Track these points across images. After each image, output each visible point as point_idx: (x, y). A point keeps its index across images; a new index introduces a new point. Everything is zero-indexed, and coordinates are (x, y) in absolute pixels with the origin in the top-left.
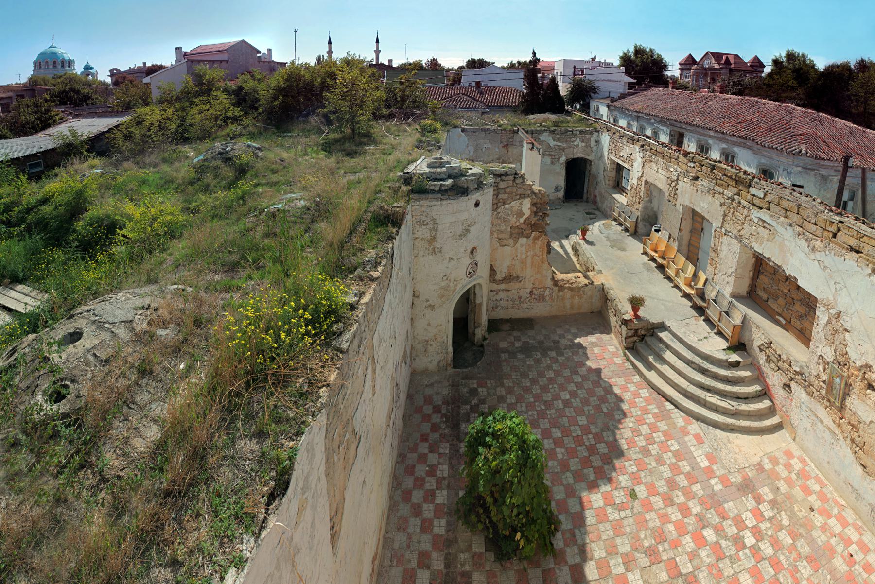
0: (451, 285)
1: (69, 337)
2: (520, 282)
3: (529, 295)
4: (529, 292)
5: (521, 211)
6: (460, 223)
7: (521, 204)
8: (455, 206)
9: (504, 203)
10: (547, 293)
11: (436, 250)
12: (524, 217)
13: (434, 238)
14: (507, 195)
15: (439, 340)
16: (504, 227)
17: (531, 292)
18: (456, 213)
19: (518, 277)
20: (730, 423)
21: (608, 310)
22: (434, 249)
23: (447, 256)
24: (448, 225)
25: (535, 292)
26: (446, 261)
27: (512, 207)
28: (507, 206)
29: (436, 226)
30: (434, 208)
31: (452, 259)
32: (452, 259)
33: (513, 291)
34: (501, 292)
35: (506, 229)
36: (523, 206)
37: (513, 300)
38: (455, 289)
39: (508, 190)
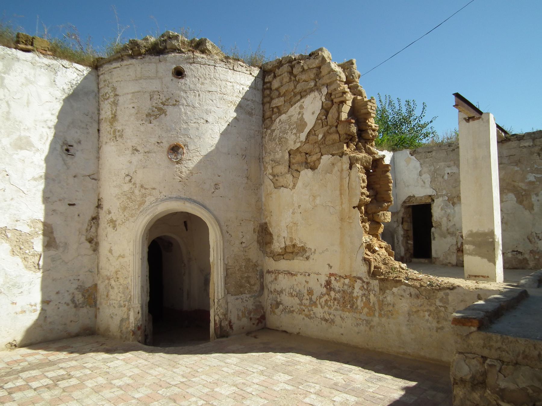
0: (137, 192)
1: (52, 252)
3: (324, 290)
4: (324, 283)
6: (147, 96)
8: (139, 69)
10: (357, 291)
12: (307, 130)
13: (115, 116)
14: (282, 99)
15: (121, 280)
17: (328, 283)
19: (303, 249)
21: (79, 84)
25: (335, 284)
27: (290, 117)
30: (115, 72)
31: (137, 151)
32: (137, 151)
35: (283, 157)
36: (304, 111)
37: (299, 295)
38: (143, 203)
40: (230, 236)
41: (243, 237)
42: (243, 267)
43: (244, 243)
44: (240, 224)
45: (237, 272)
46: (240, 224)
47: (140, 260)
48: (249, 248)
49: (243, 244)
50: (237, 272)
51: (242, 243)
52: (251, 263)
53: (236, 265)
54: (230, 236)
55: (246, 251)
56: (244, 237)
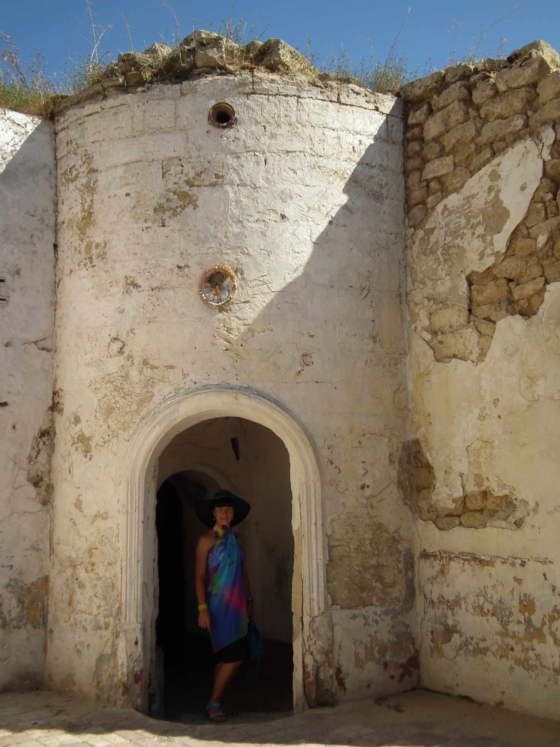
0: (134, 375)
2: (518, 524)
5: (496, 203)
6: (156, 169)
7: (495, 176)
8: (139, 113)
9: (445, 192)
11: (94, 251)
12: (509, 227)
14: (449, 160)
16: (448, 284)
18: (142, 133)
20: (295, 660)
22: (89, 247)
23: (120, 272)
24: (120, 172)
26: (117, 290)
27: (468, 199)
28: (453, 200)
29: (95, 175)
30: (90, 123)
31: (136, 286)
32: (136, 286)
33: (499, 570)
34: (455, 566)
35: (454, 289)
38: (149, 397)
39: (450, 141)
40: (336, 471)
41: (367, 472)
42: (368, 542)
43: (368, 487)
44: (360, 443)
45: (354, 555)
46: (360, 443)
47: (141, 525)
48: (379, 498)
49: (366, 489)
50: (354, 555)
51: (363, 487)
52: (384, 534)
53: (351, 539)
54: (336, 471)
55: (372, 507)
56: (368, 474)
